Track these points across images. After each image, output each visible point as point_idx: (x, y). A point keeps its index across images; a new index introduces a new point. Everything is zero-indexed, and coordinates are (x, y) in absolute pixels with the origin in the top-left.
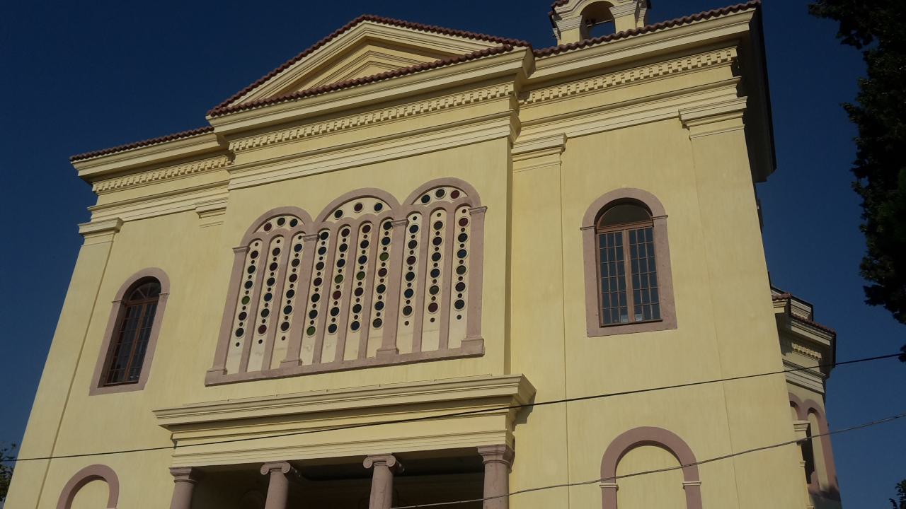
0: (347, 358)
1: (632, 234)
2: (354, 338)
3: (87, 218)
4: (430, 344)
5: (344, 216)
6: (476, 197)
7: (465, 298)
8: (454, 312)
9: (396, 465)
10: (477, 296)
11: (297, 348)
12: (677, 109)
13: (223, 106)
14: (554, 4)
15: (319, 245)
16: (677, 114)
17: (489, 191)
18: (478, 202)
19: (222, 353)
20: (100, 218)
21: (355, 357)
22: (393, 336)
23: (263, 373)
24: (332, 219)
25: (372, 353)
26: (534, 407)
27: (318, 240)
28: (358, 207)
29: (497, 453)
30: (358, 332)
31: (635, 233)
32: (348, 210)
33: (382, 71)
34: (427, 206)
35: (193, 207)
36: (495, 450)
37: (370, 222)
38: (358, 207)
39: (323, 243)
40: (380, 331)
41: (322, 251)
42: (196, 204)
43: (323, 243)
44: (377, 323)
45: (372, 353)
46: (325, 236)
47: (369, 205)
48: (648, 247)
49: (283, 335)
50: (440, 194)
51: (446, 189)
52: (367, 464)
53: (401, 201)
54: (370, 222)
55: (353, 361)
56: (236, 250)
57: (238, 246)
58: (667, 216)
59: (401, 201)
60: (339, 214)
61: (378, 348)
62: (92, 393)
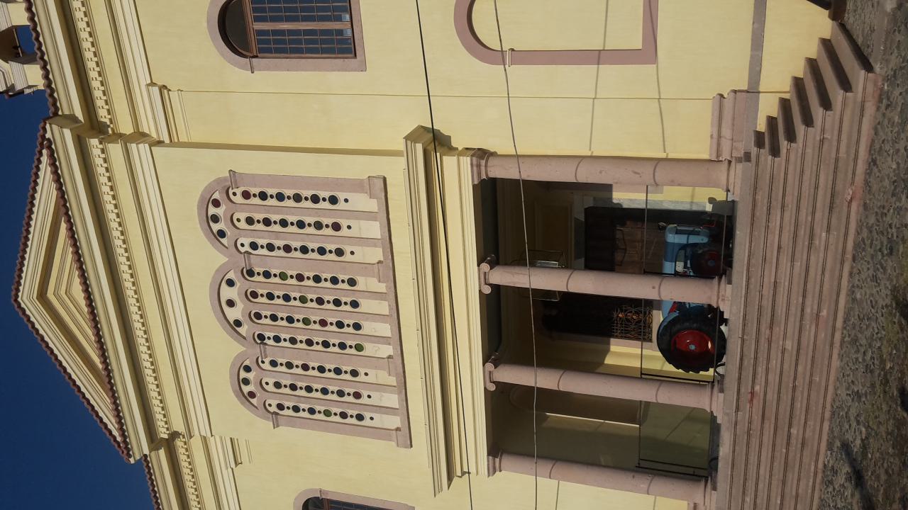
2: (366, 305)
4: (374, 229)
5: (240, 318)
6: (218, 181)
8: (341, 205)
9: (489, 263)
10: (326, 182)
15: (271, 342)
17: (216, 166)
18: (225, 179)
19: (381, 433)
21: (388, 326)
22: (365, 267)
23: (399, 393)
25: (382, 287)
27: (266, 344)
28: (231, 303)
32: (233, 314)
34: (228, 233)
35: (230, 470)
38: (231, 303)
39: (269, 338)
41: (277, 339)
43: (269, 338)
44: (352, 282)
45: (382, 287)
46: (261, 337)
47: (227, 293)
49: (368, 419)
50: (215, 219)
52: (487, 290)
55: (390, 306)
56: (276, 425)
60: (238, 323)
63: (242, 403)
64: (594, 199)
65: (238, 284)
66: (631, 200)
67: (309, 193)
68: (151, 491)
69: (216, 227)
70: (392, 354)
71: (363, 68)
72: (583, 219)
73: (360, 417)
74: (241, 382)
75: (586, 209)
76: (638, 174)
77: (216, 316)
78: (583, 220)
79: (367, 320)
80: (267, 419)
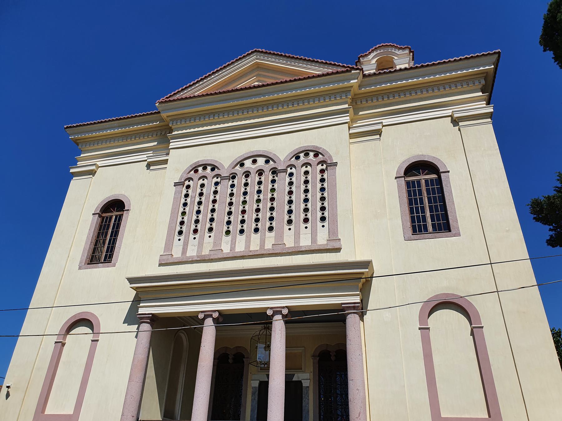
0: (252, 248)
1: (426, 181)
2: (255, 238)
3: (74, 163)
4: (305, 242)
5: (246, 166)
6: (330, 157)
7: (326, 214)
8: (303, 226)
9: (218, 318)
11: (217, 242)
12: (451, 111)
13: (167, 98)
14: (360, 55)
15: (231, 183)
16: (450, 114)
18: (331, 159)
19: (169, 245)
20: (83, 165)
21: (243, 249)
22: (280, 236)
23: (198, 256)
24: (238, 167)
26: (132, 300)
27: (229, 180)
28: (254, 162)
29: (354, 308)
30: (259, 235)
31: (428, 181)
33: (274, 81)
35: (146, 159)
36: (353, 307)
37: (237, 176)
38: (254, 162)
39: (233, 182)
40: (273, 234)
41: (233, 186)
42: (147, 157)
43: (233, 182)
44: (271, 229)
46: (234, 177)
48: (412, 196)
49: (209, 235)
51: (271, 162)
52: (269, 312)
53: (282, 158)
54: (237, 176)
55: (257, 250)
56: (176, 184)
57: (178, 182)
58: (448, 172)
59: (282, 158)
60: (242, 165)
61: (273, 243)
62: (80, 268)
63: (191, 166)
64: (308, 387)
65: (254, 166)
66: (308, 412)
67: (326, 204)
68: (101, 120)
69: (302, 155)
70: (174, 257)
71: (458, 235)
72: (294, 379)
73: (180, 233)
74: (295, 156)
75: (301, 381)
76: (359, 416)
77: (247, 153)
78: (293, 380)
79: (247, 237)
80: (181, 179)
